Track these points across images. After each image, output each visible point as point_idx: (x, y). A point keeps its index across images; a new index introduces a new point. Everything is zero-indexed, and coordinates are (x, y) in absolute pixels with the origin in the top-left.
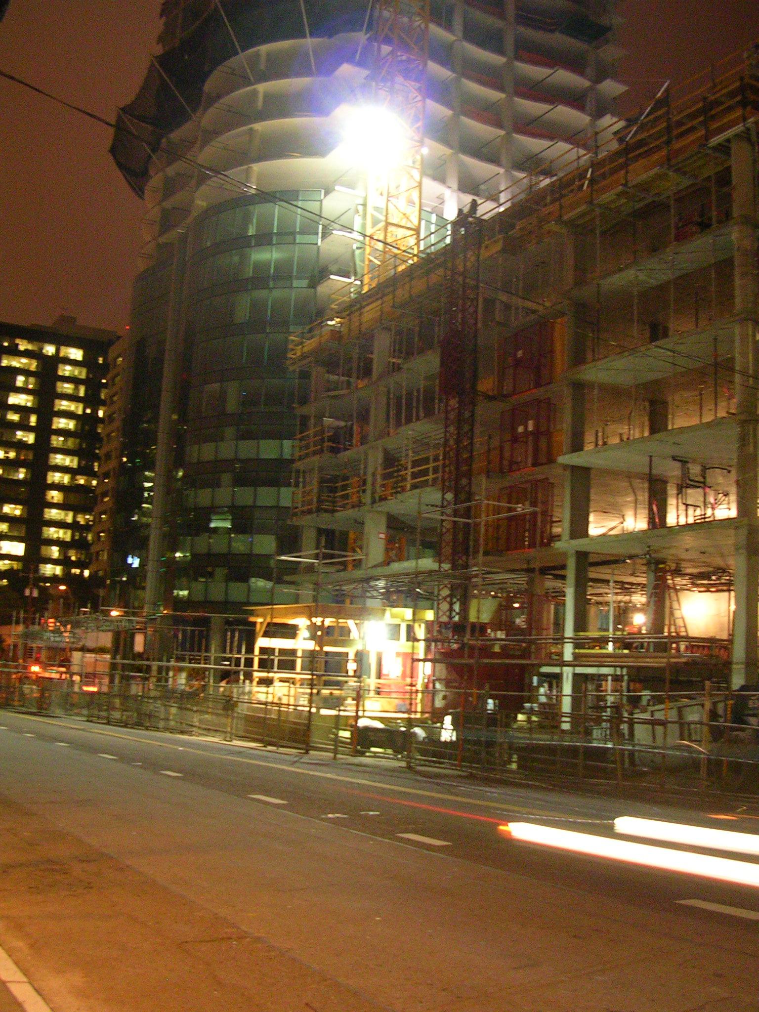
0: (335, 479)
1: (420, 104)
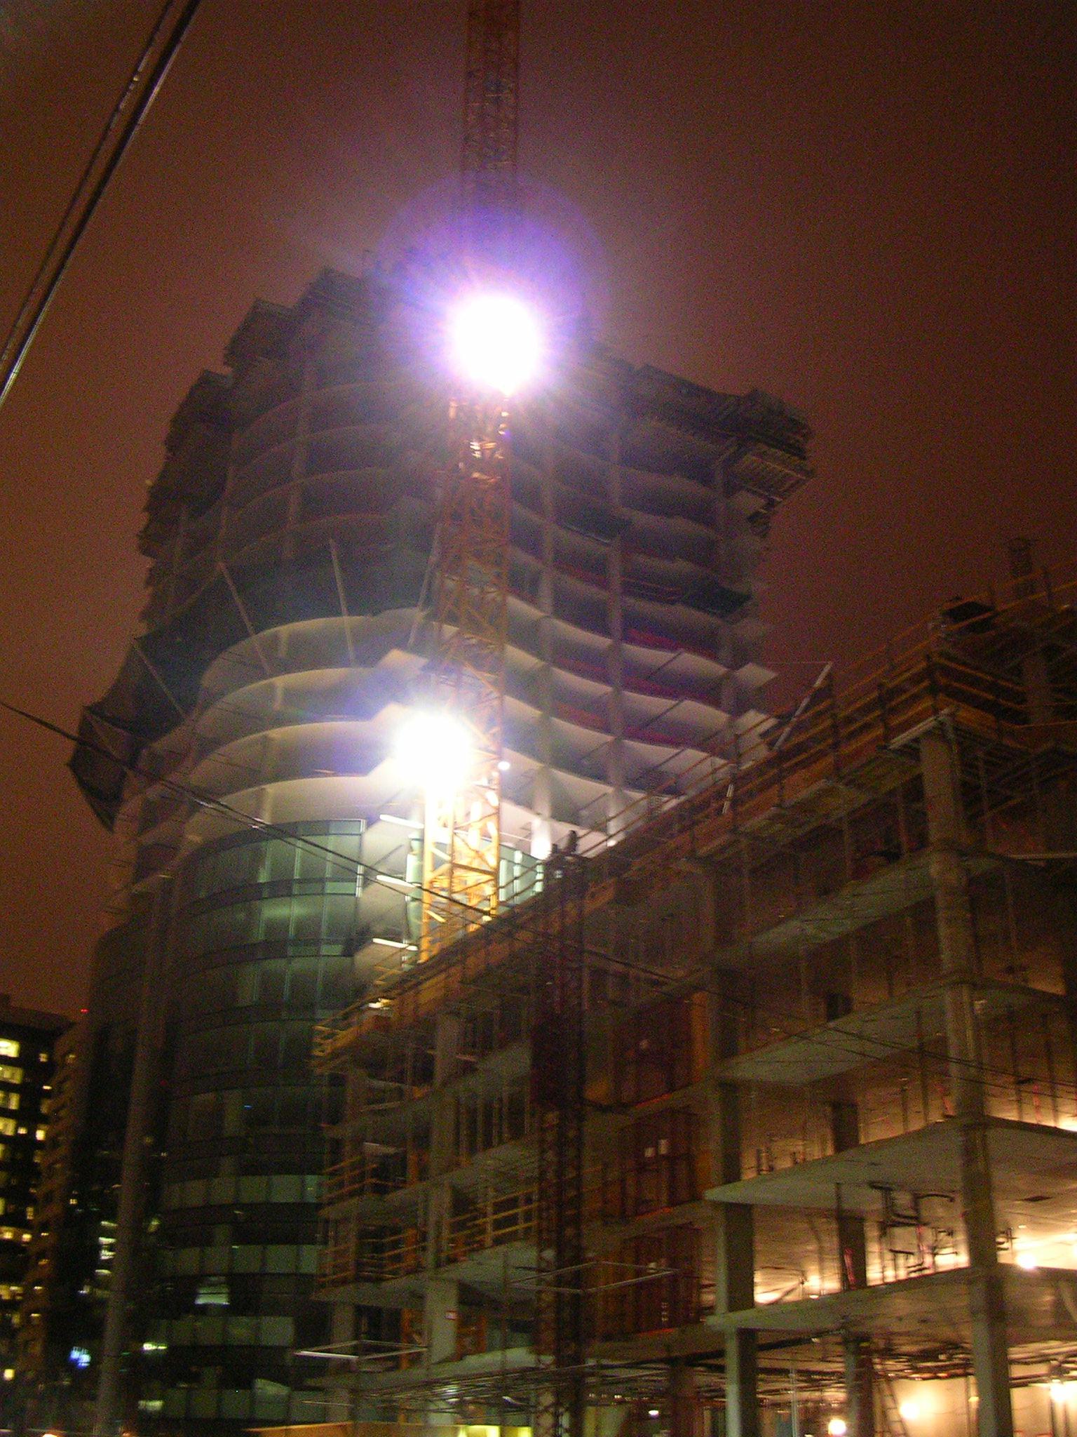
0: (380, 1232)
1: (496, 703)
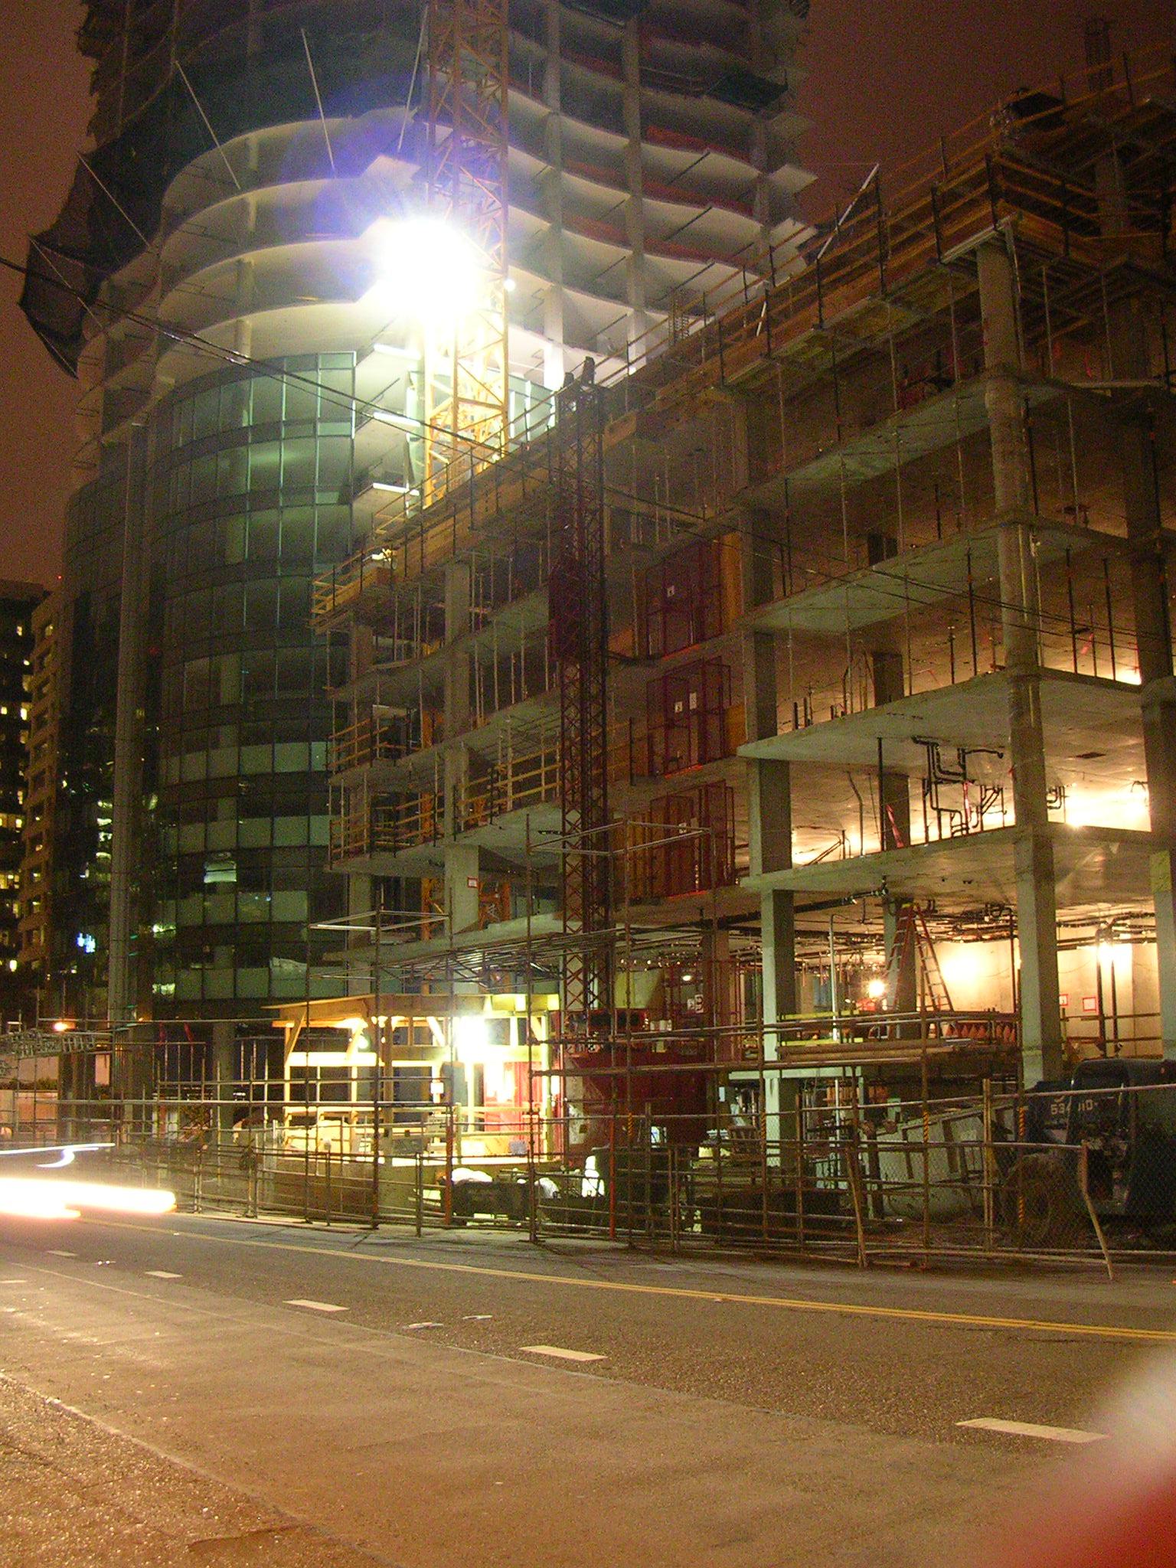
0: (395, 798)
